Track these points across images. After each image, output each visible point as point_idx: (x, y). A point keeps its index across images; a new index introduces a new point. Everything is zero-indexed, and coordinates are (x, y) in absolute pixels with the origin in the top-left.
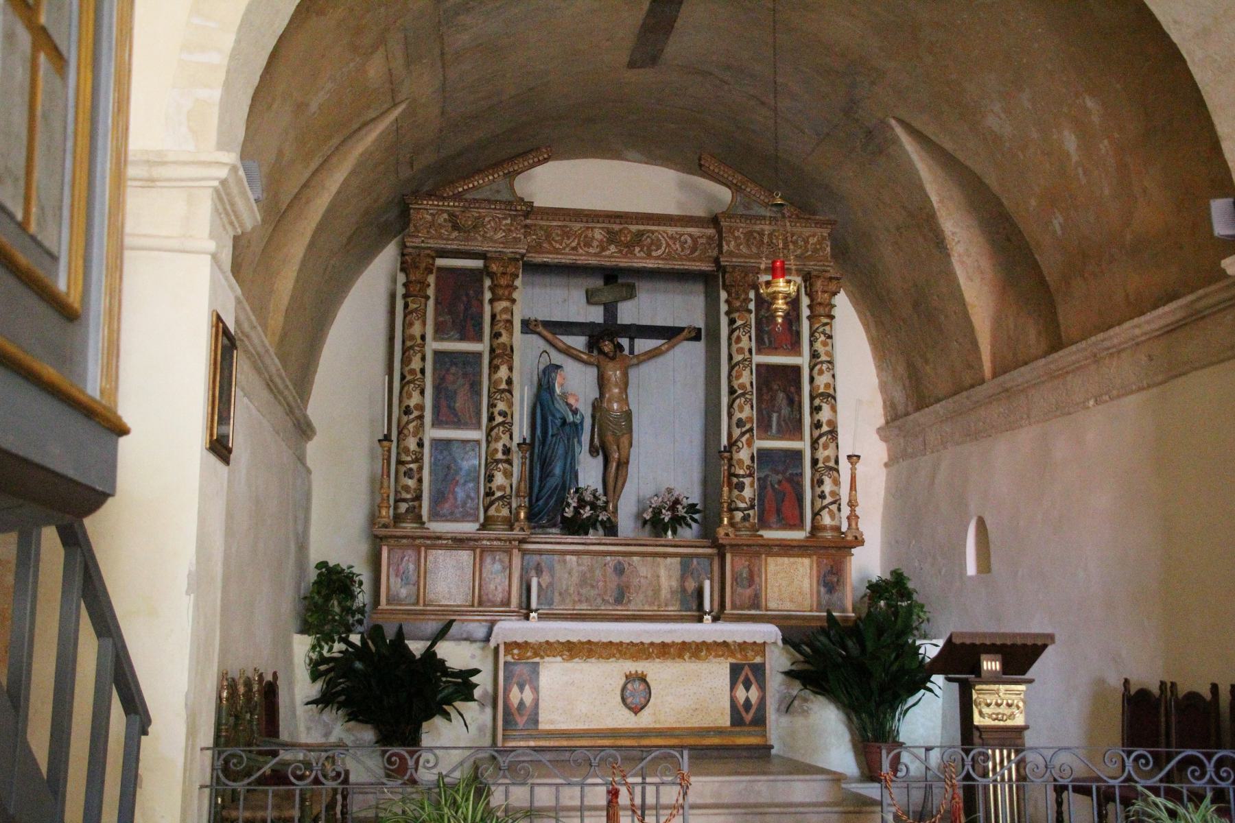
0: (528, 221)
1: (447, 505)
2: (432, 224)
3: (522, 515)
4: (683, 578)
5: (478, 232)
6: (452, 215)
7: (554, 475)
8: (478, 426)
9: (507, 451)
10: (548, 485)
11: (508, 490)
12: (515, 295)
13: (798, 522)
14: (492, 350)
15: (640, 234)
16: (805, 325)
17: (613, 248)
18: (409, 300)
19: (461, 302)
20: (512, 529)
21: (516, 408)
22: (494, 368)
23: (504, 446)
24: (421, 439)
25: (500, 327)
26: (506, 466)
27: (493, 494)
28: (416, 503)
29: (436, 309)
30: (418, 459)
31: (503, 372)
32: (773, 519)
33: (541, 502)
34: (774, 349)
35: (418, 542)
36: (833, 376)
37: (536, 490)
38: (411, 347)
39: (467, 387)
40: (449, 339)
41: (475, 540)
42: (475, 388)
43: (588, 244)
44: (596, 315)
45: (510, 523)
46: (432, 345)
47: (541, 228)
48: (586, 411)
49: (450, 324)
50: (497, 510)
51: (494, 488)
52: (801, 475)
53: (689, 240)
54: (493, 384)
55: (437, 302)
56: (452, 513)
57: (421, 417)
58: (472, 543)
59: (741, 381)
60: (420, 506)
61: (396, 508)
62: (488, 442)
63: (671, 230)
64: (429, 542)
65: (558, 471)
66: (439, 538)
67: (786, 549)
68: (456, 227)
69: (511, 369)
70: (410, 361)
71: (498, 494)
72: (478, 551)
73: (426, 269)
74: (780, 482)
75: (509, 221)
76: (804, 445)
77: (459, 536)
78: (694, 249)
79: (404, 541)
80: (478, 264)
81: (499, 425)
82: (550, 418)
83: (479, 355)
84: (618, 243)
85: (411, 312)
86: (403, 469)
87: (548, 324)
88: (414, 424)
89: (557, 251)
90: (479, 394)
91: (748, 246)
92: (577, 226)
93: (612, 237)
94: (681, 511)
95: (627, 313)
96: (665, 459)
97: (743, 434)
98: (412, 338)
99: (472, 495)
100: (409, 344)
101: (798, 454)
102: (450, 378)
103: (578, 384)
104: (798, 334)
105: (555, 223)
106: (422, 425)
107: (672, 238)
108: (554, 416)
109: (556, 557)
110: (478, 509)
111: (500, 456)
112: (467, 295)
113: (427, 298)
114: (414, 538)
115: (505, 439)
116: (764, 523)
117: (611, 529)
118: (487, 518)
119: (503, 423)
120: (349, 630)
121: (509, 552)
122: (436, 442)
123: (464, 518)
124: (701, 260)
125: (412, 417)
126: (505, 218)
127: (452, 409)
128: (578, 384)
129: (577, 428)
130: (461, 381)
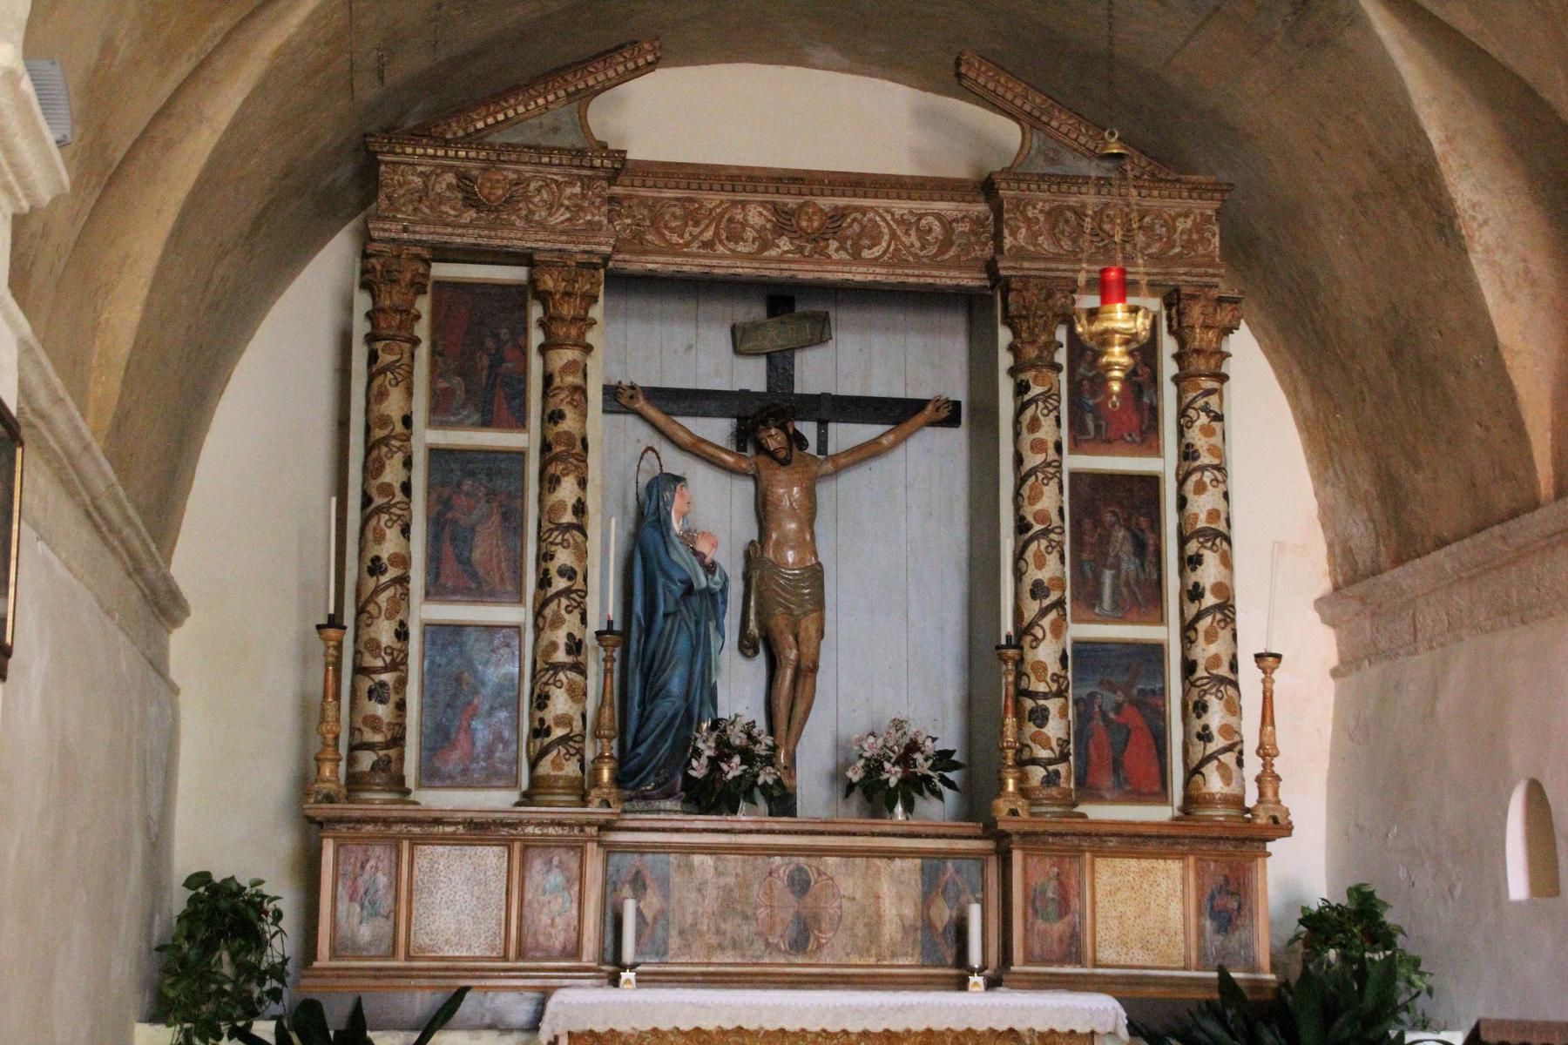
0: (617, 190)
1: (455, 755)
4: (926, 901)
6: (463, 177)
7: (668, 695)
8: (519, 599)
9: (575, 646)
10: (657, 714)
11: (577, 725)
13: (1157, 788)
14: (546, 447)
15: (839, 215)
16: (1169, 393)
17: (785, 244)
18: (379, 345)
21: (594, 561)
22: (549, 482)
23: (570, 636)
24: (402, 624)
25: (561, 401)
26: (573, 675)
27: (548, 732)
28: (393, 753)
29: (433, 365)
30: (398, 664)
31: (567, 490)
32: (1106, 781)
33: (642, 750)
34: (1105, 442)
35: (396, 829)
36: (1226, 496)
38: (384, 441)
39: (496, 518)
40: (459, 425)
42: (512, 521)
43: (735, 237)
44: (752, 376)
46: (426, 436)
47: (643, 202)
48: (732, 567)
50: (556, 765)
51: (549, 721)
52: (1162, 693)
53: (937, 227)
54: (548, 513)
55: (435, 351)
57: (403, 580)
58: (504, 831)
59: (1038, 506)
60: (401, 758)
61: (352, 761)
62: (538, 630)
63: (902, 207)
64: (417, 830)
65: (676, 685)
66: (438, 821)
67: (1135, 842)
68: (471, 201)
69: (582, 483)
70: (380, 470)
72: (517, 846)
73: (413, 283)
74: (1118, 708)
76: (1168, 634)
78: (946, 244)
79: (369, 828)
80: (515, 274)
81: (559, 594)
82: (661, 580)
83: (519, 456)
84: (797, 234)
85: (382, 371)
86: (366, 684)
87: (657, 395)
88: (390, 592)
89: (673, 250)
90: (519, 531)
91: (1057, 243)
92: (713, 200)
93: (784, 221)
94: (922, 766)
95: (816, 372)
96: (886, 665)
97: (1044, 612)
98: (385, 421)
99: (506, 734)
100: (378, 433)
101: (1156, 652)
102: (462, 502)
103: (716, 512)
104: (1154, 412)
106: (406, 593)
107: (901, 221)
108: (669, 577)
109: (672, 858)
110: (517, 761)
111: (561, 656)
112: (496, 336)
113: (416, 342)
114: (387, 822)
115: (571, 622)
116: (1087, 789)
117: (782, 801)
119: (566, 592)
120: (252, 1014)
121: (579, 849)
122: (434, 631)
124: (956, 264)
125: (384, 579)
126: (572, 184)
127: (465, 562)
128: (716, 512)
129: (714, 600)
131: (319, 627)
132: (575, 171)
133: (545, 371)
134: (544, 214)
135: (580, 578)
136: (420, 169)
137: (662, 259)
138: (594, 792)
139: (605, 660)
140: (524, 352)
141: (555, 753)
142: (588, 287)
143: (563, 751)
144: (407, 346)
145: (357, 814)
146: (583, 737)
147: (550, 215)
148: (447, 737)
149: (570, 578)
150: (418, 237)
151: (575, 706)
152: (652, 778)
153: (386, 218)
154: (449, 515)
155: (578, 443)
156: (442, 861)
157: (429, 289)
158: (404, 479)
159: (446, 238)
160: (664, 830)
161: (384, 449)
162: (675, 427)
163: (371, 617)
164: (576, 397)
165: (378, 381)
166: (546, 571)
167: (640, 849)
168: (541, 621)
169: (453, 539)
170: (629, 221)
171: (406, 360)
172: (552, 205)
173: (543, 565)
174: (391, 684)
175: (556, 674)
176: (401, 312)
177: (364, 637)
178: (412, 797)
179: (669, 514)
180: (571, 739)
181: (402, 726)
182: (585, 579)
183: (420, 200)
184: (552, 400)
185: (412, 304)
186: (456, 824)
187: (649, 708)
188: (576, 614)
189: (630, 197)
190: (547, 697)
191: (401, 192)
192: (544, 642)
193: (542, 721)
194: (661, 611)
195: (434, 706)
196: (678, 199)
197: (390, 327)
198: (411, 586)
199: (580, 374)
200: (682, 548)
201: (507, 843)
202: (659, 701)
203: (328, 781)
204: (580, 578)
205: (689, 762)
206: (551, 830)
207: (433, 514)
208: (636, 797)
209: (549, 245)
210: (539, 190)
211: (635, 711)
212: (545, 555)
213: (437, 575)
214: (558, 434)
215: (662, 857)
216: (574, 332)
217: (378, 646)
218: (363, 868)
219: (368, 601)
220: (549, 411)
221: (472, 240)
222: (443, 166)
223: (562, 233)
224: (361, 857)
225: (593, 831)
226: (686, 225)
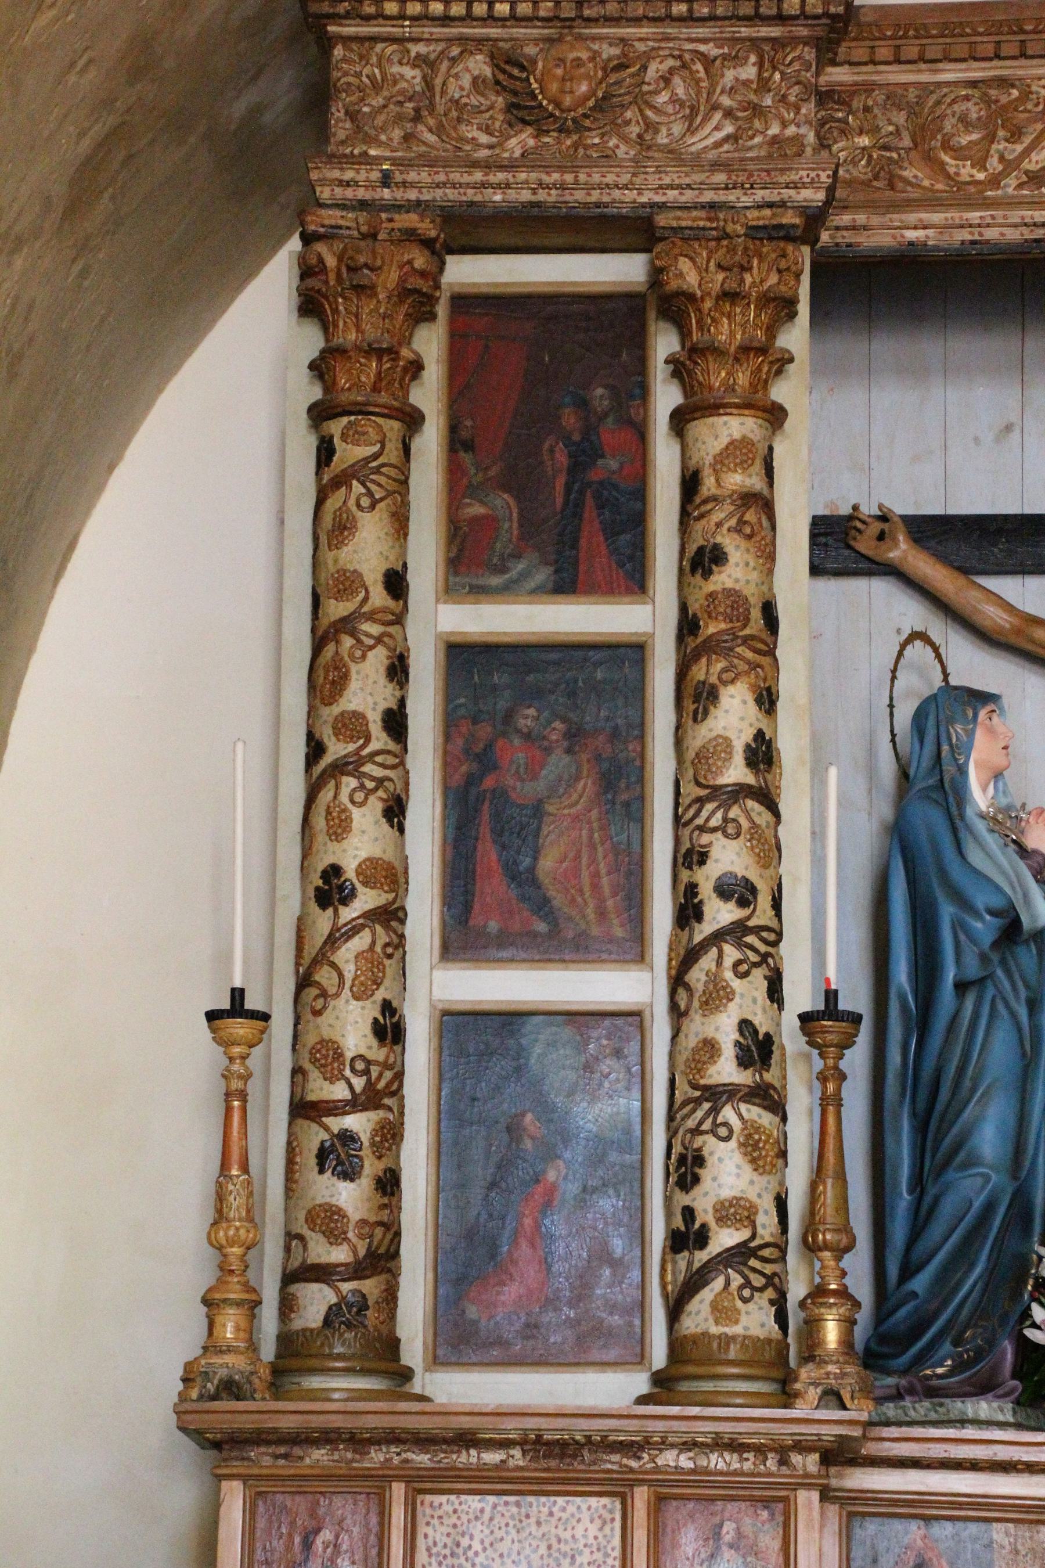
0: (839, 75)
1: (511, 1292)
2: (423, 104)
3: (831, 1333)
5: (617, 127)
7: (973, 1161)
8: (636, 951)
9: (757, 1049)
10: (948, 1207)
11: (767, 1224)
12: (781, 392)
14: (688, 625)
18: (336, 427)
19: (550, 436)
20: (786, 1394)
21: (795, 869)
22: (696, 699)
23: (745, 1025)
24: (388, 1008)
25: (719, 526)
26: (753, 1112)
27: (702, 1239)
28: (371, 1287)
29: (454, 472)
30: (382, 1093)
31: (734, 715)
33: (920, 1283)
35: (377, 1456)
37: (898, 1231)
38: (346, 625)
39: (587, 786)
40: (506, 591)
41: (630, 1448)
42: (621, 785)
45: (777, 1372)
47: (894, 97)
49: (510, 528)
50: (720, 1311)
51: (705, 1214)
54: (695, 764)
55: (457, 442)
56: (531, 1329)
57: (391, 916)
58: (613, 1461)
60: (391, 1296)
61: (287, 1306)
62: (677, 1014)
64: (422, 1459)
65: (989, 1139)
66: (467, 1440)
68: (523, 111)
69: (767, 700)
70: (339, 683)
71: (725, 1238)
72: (641, 1496)
73: (403, 293)
75: (749, 72)
77: (553, 1429)
79: (319, 1455)
80: (620, 270)
81: (718, 937)
82: (947, 911)
83: (633, 652)
85: (341, 481)
86: (314, 1136)
87: (934, 531)
88: (360, 942)
90: (636, 811)
98: (348, 583)
99: (618, 1245)
100: (336, 609)
102: (515, 754)
105: (950, 73)
106: (399, 942)
108: (963, 903)
109: (999, 1533)
110: (642, 1306)
111: (726, 1070)
112: (583, 404)
113: (413, 420)
114: (359, 1441)
115: (748, 997)
118: (679, 1348)
119: (737, 931)
121: (778, 1502)
122: (458, 1025)
123: (586, 1346)
125: (349, 913)
126: (736, 60)
127: (524, 879)
130: (558, 763)
131: (212, 1016)
132: (745, 31)
133: (684, 467)
134: (677, 129)
135: (764, 901)
136: (415, 49)
137: (937, 218)
138: (807, 1373)
139: (823, 1078)
140: (641, 433)
141: (719, 1283)
142: (773, 279)
143: (737, 1280)
144: (393, 428)
145: (287, 1423)
146: (783, 1251)
147: (691, 130)
148: (493, 1254)
149: (743, 903)
150: (412, 195)
151: (762, 1181)
152: (947, 1347)
153: (351, 160)
154: (489, 782)
155: (756, 614)
156: (478, 1530)
157: (442, 310)
158: (393, 704)
159: (471, 195)
160: (973, 1466)
161: (348, 642)
162: (974, 594)
163: (324, 994)
164: (750, 516)
165: (333, 503)
166: (692, 889)
167: (921, 1509)
168: (682, 996)
169: (498, 833)
170: (865, 141)
171: (392, 454)
172: (694, 110)
173: (685, 875)
174: (365, 1138)
175: (715, 1110)
176: (379, 353)
177: (310, 1039)
178: (417, 1386)
179: (962, 770)
180: (754, 1253)
181: (393, 1230)
182: (777, 905)
183: (417, 118)
184: (699, 527)
185: (407, 340)
186: (505, 1444)
187: (932, 1191)
188: (759, 978)
189: (868, 88)
190: (699, 1160)
191: (378, 101)
192: (690, 1041)
193: (689, 1213)
194: (950, 975)
195: (461, 1186)
196: (974, 84)
197: (357, 385)
198: (409, 930)
199: (758, 466)
200: (992, 842)
201: (620, 1488)
202: (951, 1175)
203: (229, 1350)
204: (764, 901)
205: (1026, 1314)
206: (716, 1461)
207: (457, 779)
208: (911, 1391)
209: (689, 196)
210: (666, 80)
211: (903, 1200)
212: (689, 852)
213: (467, 907)
214: (712, 595)
215: (973, 1528)
216: (743, 378)
217: (339, 1055)
218: (307, 1545)
219: (316, 962)
220: (692, 549)
221: (526, 196)
222: (461, 39)
223: (716, 166)
224: (303, 1520)
225: (811, 1462)
226: (991, 138)
